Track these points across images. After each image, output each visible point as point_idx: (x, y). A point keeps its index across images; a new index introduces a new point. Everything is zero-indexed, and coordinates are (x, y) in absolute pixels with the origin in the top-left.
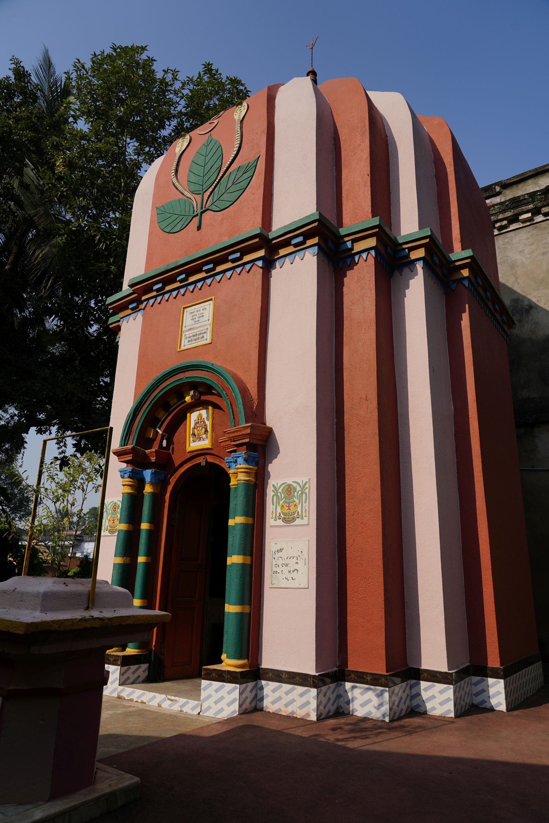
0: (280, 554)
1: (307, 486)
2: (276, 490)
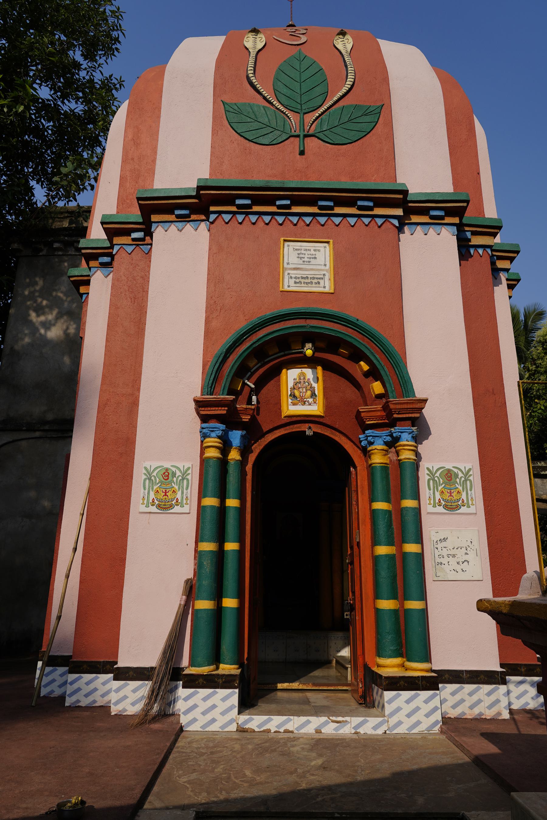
1: (190, 471)
2: (431, 474)
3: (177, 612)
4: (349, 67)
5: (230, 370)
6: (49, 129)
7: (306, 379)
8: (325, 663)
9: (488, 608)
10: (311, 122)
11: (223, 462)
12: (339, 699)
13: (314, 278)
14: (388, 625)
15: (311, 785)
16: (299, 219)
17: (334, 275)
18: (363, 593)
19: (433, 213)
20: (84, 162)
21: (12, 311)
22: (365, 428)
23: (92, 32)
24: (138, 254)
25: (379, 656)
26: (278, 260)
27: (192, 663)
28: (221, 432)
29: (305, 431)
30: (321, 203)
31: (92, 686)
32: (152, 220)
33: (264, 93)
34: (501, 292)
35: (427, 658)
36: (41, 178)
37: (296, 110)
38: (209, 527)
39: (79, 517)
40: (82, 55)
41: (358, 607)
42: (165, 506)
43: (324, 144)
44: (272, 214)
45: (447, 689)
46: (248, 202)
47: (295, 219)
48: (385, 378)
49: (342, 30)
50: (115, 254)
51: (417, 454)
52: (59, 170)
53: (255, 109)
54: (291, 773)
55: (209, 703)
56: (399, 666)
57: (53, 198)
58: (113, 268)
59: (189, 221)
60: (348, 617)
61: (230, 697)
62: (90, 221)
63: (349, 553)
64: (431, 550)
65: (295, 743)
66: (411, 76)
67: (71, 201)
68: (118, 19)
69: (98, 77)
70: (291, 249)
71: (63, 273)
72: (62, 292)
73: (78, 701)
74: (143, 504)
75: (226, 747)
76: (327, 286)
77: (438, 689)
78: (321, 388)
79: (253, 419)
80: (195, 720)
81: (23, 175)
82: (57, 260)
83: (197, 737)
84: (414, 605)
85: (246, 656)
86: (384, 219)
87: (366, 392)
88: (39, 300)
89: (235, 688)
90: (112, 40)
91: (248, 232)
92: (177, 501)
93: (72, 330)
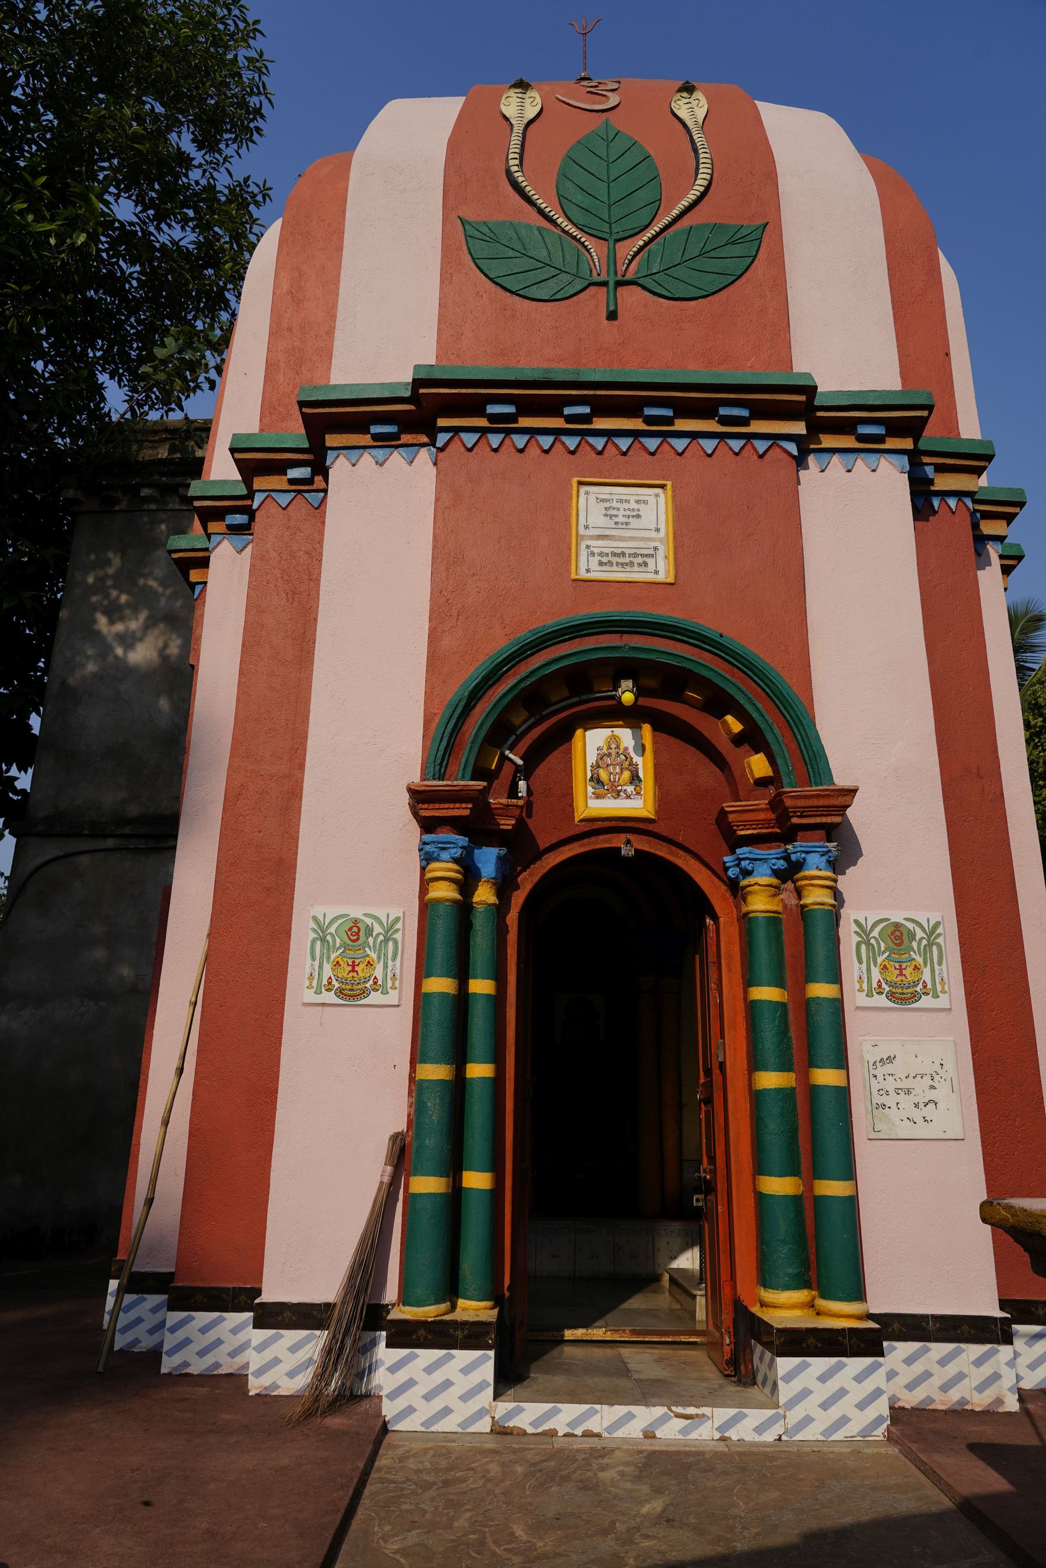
0: (888, 1068)
1: (399, 926)
3: (376, 1197)
4: (700, 151)
5: (477, 732)
6: (134, 279)
7: (622, 748)
8: (647, 1281)
9: (1008, 1220)
10: (629, 257)
11: (464, 909)
12: (685, 1363)
13: (636, 555)
14: (782, 1226)
15: (644, 1561)
16: (607, 442)
17: (676, 548)
18: (732, 1160)
19: (864, 430)
20: (196, 339)
21: (63, 614)
22: (735, 843)
23: (212, 98)
24: (300, 509)
25: (765, 1286)
26: (567, 520)
27: (405, 1298)
28: (460, 851)
29: (620, 849)
30: (649, 411)
31: (211, 1336)
32: (328, 444)
33: (540, 201)
34: (990, 580)
35: (858, 1293)
36: (118, 368)
37: (600, 235)
38: (438, 1035)
39: (187, 1009)
40: (193, 141)
41: (721, 1186)
42: (351, 992)
43: (655, 298)
44: (557, 432)
45: (899, 1351)
46: (510, 409)
47: (599, 443)
48: (774, 747)
49: (687, 82)
50: (257, 510)
51: (837, 895)
52: (151, 352)
53: (523, 232)
54: (605, 1532)
55: (438, 1377)
56: (802, 1306)
57: (140, 406)
58: (252, 534)
59: (397, 447)
60: (700, 1204)
61: (477, 1366)
62: (209, 446)
63: (702, 1081)
64: (864, 1079)
65: (606, 1461)
66: (819, 172)
67: (173, 410)
68: (261, 73)
69: (222, 181)
70: (592, 499)
71: (158, 543)
72: (155, 579)
73: (186, 1364)
74: (310, 987)
75: (473, 1469)
76: (661, 569)
77: (881, 1354)
78: (650, 765)
79: (521, 825)
80: (410, 1410)
81: (87, 363)
82: (146, 519)
83: (416, 1446)
84: (832, 1188)
85: (507, 1282)
86: (770, 442)
87: (737, 774)
88: (114, 593)
89: (488, 1347)
90: (248, 112)
91: (510, 466)
92: (375, 983)
93: (174, 650)
